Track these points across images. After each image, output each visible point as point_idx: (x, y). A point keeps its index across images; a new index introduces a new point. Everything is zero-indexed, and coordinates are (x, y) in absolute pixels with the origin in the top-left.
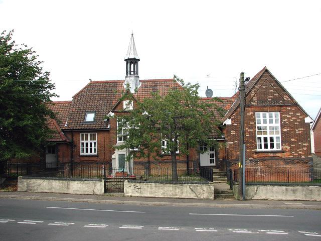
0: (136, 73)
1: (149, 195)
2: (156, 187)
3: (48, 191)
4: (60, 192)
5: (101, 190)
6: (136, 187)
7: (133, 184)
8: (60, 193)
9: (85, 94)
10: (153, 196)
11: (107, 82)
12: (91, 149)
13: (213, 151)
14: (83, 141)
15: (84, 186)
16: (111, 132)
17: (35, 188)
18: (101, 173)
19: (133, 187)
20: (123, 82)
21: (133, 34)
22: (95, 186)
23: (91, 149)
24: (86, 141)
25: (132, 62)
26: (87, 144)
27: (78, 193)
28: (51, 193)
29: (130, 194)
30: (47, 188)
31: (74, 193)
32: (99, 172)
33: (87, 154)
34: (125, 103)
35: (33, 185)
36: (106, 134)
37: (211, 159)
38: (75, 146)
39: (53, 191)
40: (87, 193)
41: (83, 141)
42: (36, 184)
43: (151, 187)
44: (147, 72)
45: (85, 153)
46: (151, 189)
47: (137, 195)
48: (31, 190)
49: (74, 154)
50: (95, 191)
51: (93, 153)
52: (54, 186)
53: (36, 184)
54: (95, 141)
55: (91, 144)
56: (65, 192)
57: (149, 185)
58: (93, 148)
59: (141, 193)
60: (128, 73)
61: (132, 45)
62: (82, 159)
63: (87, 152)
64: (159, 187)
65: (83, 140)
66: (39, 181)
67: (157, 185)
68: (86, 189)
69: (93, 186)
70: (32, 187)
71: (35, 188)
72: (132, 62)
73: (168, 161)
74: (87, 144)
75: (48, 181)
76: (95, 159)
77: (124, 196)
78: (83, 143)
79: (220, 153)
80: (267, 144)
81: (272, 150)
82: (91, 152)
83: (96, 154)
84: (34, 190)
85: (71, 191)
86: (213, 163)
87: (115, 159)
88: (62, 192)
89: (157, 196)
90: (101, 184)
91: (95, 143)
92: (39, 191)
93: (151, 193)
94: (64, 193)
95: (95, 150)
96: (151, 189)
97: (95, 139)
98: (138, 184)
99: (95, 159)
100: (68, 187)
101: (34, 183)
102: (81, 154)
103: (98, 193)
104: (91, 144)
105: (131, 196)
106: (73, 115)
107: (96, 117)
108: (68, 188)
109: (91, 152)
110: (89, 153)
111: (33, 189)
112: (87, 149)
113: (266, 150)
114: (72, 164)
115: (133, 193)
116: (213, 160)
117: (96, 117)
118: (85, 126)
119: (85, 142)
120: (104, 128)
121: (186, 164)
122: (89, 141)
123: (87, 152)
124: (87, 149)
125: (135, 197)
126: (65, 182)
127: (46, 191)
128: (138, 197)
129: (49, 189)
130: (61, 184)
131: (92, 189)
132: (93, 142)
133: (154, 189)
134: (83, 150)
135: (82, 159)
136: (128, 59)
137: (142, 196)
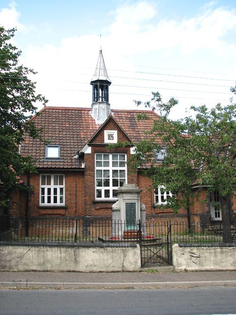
0: (106, 98)
1: (212, 267)
2: (222, 252)
3: (39, 268)
4: (62, 269)
5: (136, 262)
6: (192, 255)
7: (188, 249)
8: (62, 271)
9: (39, 122)
10: (218, 268)
11: (67, 110)
12: (55, 198)
13: (218, 201)
14: (43, 186)
15: (106, 257)
16: (87, 173)
17: (13, 263)
18: (71, 232)
19: (187, 256)
20: (89, 110)
21: (101, 51)
22: (125, 256)
23: (55, 198)
24: (49, 187)
25: (101, 87)
26: (49, 190)
27: (95, 269)
28: (44, 271)
29: (183, 268)
30: (36, 262)
31: (89, 269)
32: (68, 231)
33: (49, 204)
34: (106, 133)
35: (8, 258)
36: (79, 180)
37: (216, 213)
38: (33, 193)
39: (49, 267)
40: (110, 269)
41: (43, 186)
42: (13, 256)
43: (215, 252)
44: (121, 99)
45: (46, 204)
46: (216, 256)
47: (195, 267)
48: (5, 267)
49: (30, 204)
50: (125, 264)
51: (58, 204)
52: (49, 257)
53: (13, 256)
54: (61, 186)
55: (55, 190)
56: (72, 269)
57: (212, 250)
58: (58, 196)
59: (200, 264)
60: (96, 99)
61: (102, 64)
62: (44, 212)
63: (49, 201)
64: (226, 252)
65: (43, 183)
66: (20, 250)
67: (224, 249)
68: (110, 261)
69: (122, 256)
70: (6, 261)
71: (13, 263)
72: (101, 87)
73: (163, 214)
74: (49, 190)
75: (37, 249)
76: (62, 212)
77: (174, 271)
78: (43, 189)
79: (234, 203)
80: (48, 194)
81: (107, 199)
82: (55, 201)
83: (63, 204)
84: (11, 267)
85: (81, 267)
86: (219, 217)
87: (119, 210)
88: (66, 269)
89: (224, 269)
90: (135, 253)
91: (61, 189)
92: (21, 268)
93: (216, 263)
94: (69, 271)
95: (61, 199)
96: (216, 256)
97: (61, 183)
98: (195, 250)
99: (62, 212)
100: (76, 259)
101: (10, 253)
102: (41, 204)
103: (131, 268)
104: (55, 190)
105: (186, 271)
106: (27, 148)
107: (62, 152)
108: (76, 261)
109: (55, 201)
110: (52, 203)
111: (8, 264)
112: (49, 198)
113: (107, 199)
114: (27, 219)
115: (188, 265)
116: (219, 213)
117: (62, 152)
118: (49, 165)
119: (46, 187)
120: (77, 167)
121: (185, 220)
122: (52, 186)
123: (49, 201)
124: (49, 198)
125: (193, 271)
126: (69, 250)
127: (35, 268)
128: (196, 271)
129: (40, 265)
130: (63, 255)
131: (121, 261)
132: (58, 187)
133: (219, 257)
134: (43, 198)
135: (44, 212)
136: (98, 81)
137: (203, 268)
